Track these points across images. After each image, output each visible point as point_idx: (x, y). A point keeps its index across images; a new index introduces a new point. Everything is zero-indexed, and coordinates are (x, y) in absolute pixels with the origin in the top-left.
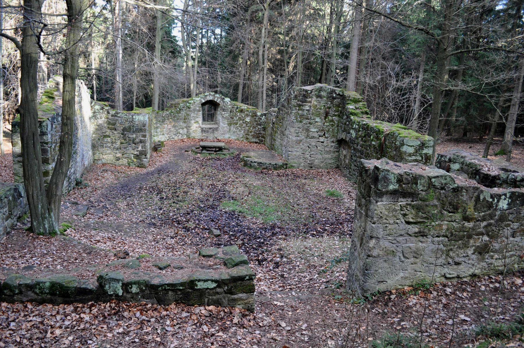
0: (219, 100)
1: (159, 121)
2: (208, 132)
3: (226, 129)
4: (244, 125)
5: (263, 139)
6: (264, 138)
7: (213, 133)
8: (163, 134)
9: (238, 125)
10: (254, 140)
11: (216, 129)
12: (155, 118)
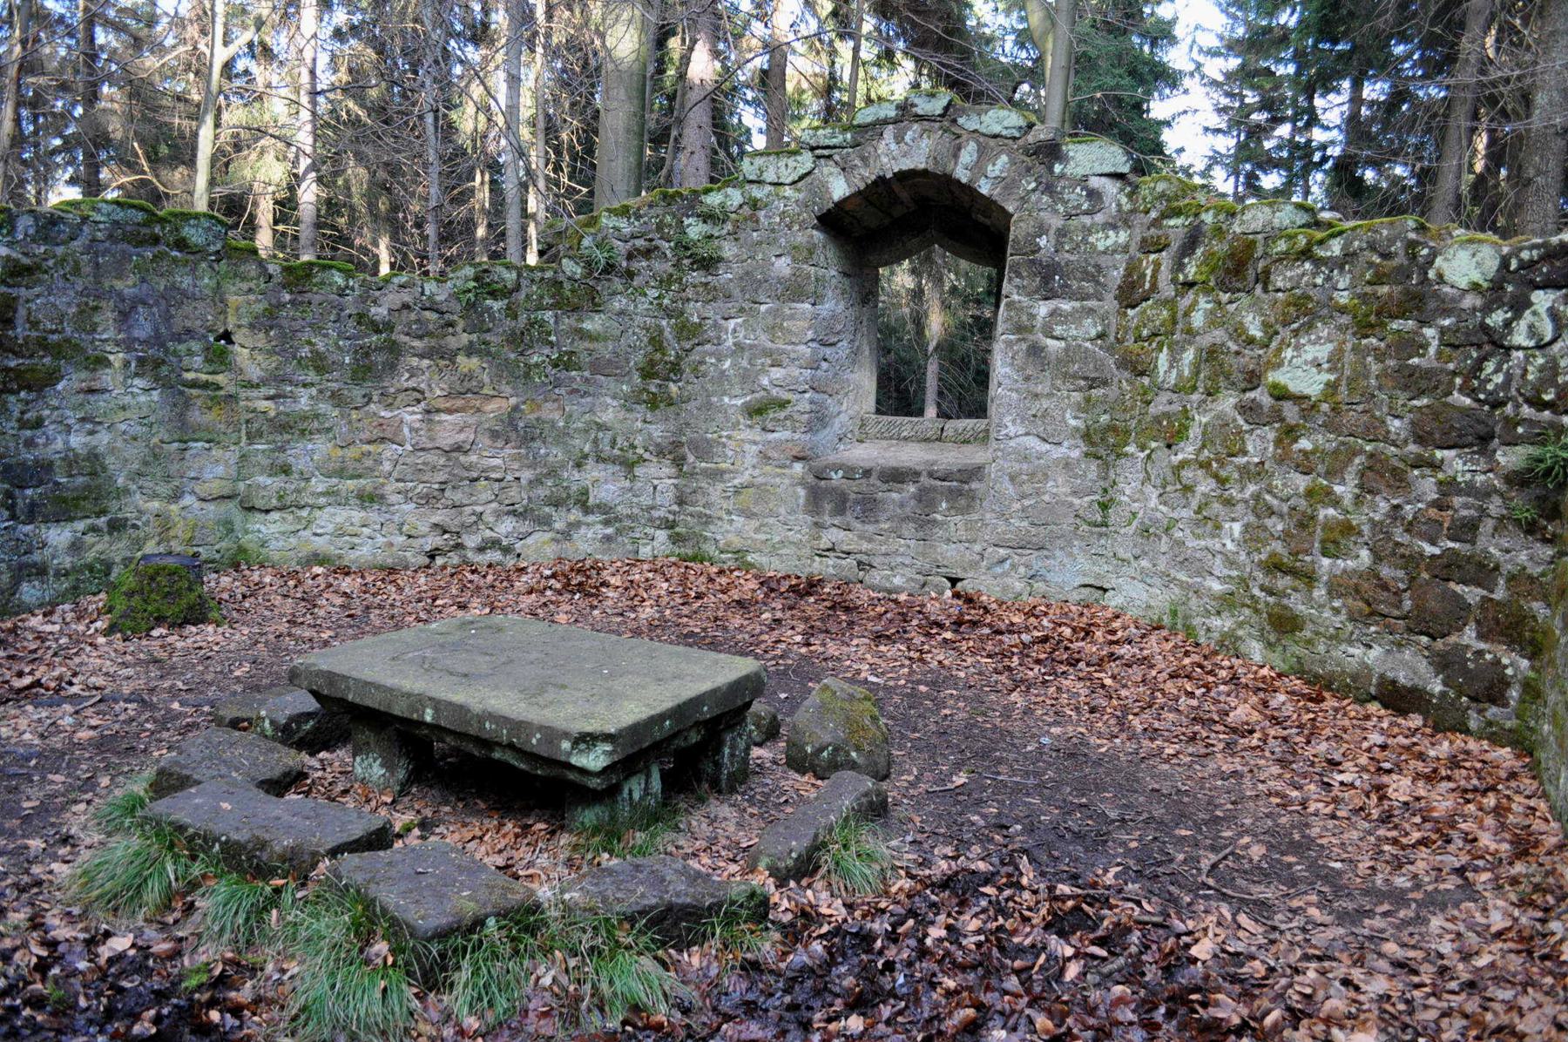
0: (1000, 165)
1: (320, 364)
2: (869, 508)
4: (1259, 444)
5: (1516, 664)
6: (1535, 649)
7: (924, 522)
8: (369, 499)
9: (1187, 451)
10: (1371, 656)
11: (961, 486)
12: (267, 321)
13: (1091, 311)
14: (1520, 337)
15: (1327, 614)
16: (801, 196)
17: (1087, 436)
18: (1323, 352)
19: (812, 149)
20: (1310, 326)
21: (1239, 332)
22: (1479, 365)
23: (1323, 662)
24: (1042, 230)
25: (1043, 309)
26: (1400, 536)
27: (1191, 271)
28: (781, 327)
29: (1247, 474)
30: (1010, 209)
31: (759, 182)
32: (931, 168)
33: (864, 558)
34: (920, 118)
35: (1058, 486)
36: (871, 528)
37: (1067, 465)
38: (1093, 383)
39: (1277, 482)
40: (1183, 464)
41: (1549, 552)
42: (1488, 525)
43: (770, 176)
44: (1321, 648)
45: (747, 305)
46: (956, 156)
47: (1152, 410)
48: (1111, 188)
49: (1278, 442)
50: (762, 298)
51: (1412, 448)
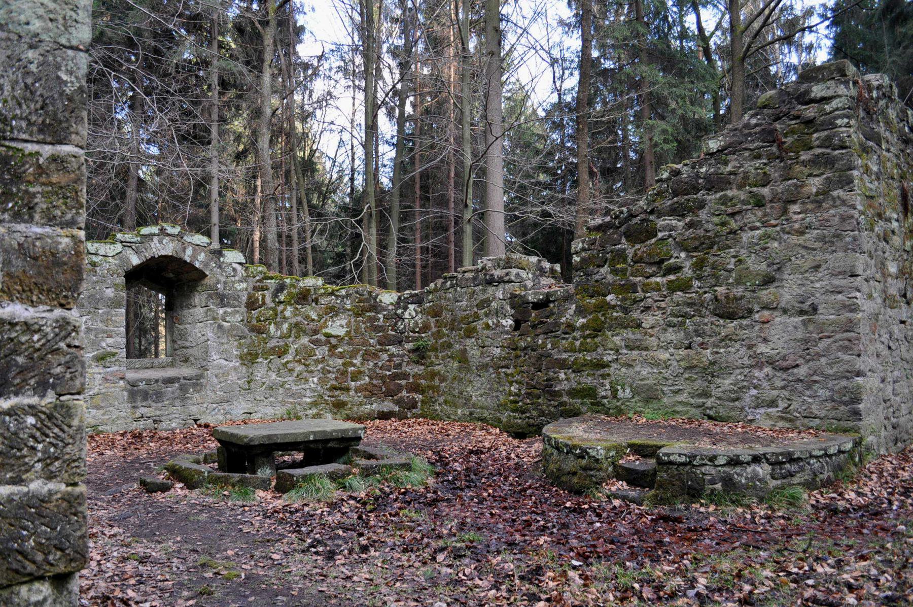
2: (159, 396)
3: (233, 377)
4: (321, 352)
5: (418, 397)
7: (184, 399)
9: (289, 357)
11: (196, 382)
13: (238, 312)
14: (406, 315)
15: (356, 398)
16: (117, 262)
17: (241, 358)
18: (344, 322)
19: (122, 242)
20: (337, 315)
21: (307, 317)
22: (396, 324)
23: (356, 413)
24: (218, 282)
25: (221, 311)
26: (378, 371)
27: (282, 298)
28: (111, 320)
29: (317, 362)
30: (207, 273)
31: (96, 254)
32: (175, 255)
33: (157, 418)
34: (168, 235)
35: (233, 377)
36: (160, 405)
37: (235, 369)
38: (241, 338)
39: (331, 363)
40: (287, 362)
41: (423, 367)
42: (404, 364)
43: (102, 252)
44: (355, 409)
45: (92, 310)
46: (184, 252)
47: (268, 345)
48: (239, 267)
49: (329, 351)
50: (100, 307)
51: (378, 347)
